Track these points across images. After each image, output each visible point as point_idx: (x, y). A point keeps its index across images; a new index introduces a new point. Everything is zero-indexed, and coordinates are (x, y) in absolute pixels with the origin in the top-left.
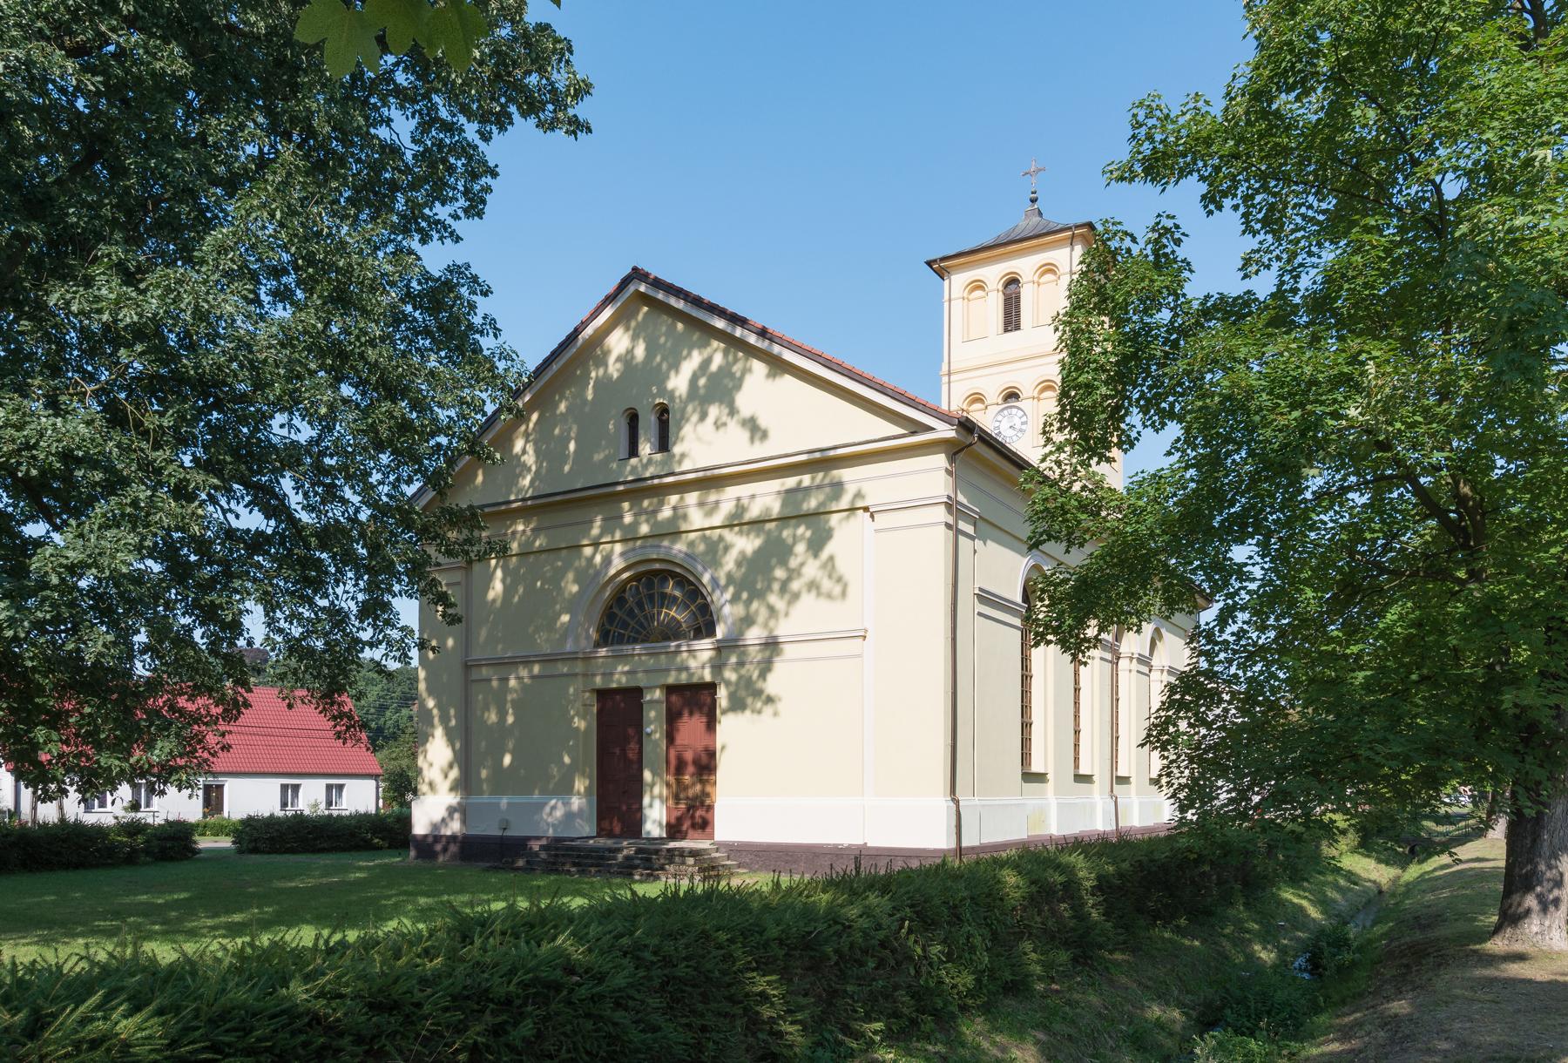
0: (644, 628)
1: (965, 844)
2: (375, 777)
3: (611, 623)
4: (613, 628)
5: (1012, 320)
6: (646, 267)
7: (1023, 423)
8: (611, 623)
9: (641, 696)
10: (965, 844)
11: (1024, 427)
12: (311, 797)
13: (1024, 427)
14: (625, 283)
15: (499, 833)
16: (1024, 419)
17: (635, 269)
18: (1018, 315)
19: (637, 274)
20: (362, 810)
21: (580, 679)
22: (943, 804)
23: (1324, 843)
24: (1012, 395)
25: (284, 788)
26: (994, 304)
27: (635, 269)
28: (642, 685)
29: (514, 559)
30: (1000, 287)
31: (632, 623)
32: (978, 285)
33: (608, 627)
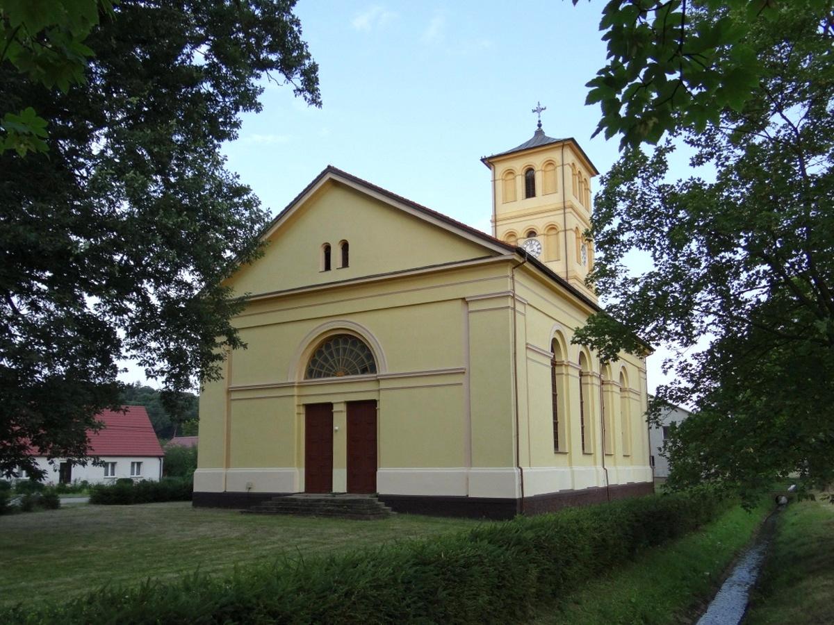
0: (334, 368)
1: (525, 496)
2: (159, 457)
3: (314, 365)
4: (315, 369)
5: (530, 192)
6: (581, 453)
7: (538, 249)
8: (314, 365)
9: (332, 409)
10: (525, 496)
11: (539, 251)
12: (123, 469)
13: (539, 251)
14: (324, 173)
15: (247, 491)
16: (539, 246)
17: (329, 167)
18: (534, 189)
19: (330, 169)
20: (154, 480)
21: (296, 398)
22: (298, 492)
23: (24, 342)
24: (532, 234)
25: (133, 464)
26: (520, 183)
27: (329, 167)
28: (332, 402)
29: (594, 469)
30: (523, 174)
31: (327, 366)
32: (510, 172)
33: (312, 367)
